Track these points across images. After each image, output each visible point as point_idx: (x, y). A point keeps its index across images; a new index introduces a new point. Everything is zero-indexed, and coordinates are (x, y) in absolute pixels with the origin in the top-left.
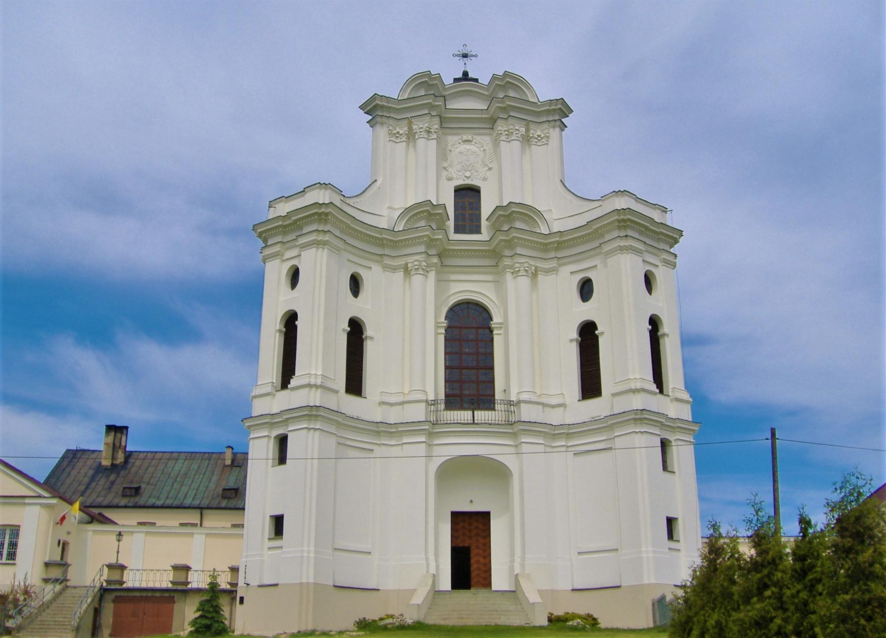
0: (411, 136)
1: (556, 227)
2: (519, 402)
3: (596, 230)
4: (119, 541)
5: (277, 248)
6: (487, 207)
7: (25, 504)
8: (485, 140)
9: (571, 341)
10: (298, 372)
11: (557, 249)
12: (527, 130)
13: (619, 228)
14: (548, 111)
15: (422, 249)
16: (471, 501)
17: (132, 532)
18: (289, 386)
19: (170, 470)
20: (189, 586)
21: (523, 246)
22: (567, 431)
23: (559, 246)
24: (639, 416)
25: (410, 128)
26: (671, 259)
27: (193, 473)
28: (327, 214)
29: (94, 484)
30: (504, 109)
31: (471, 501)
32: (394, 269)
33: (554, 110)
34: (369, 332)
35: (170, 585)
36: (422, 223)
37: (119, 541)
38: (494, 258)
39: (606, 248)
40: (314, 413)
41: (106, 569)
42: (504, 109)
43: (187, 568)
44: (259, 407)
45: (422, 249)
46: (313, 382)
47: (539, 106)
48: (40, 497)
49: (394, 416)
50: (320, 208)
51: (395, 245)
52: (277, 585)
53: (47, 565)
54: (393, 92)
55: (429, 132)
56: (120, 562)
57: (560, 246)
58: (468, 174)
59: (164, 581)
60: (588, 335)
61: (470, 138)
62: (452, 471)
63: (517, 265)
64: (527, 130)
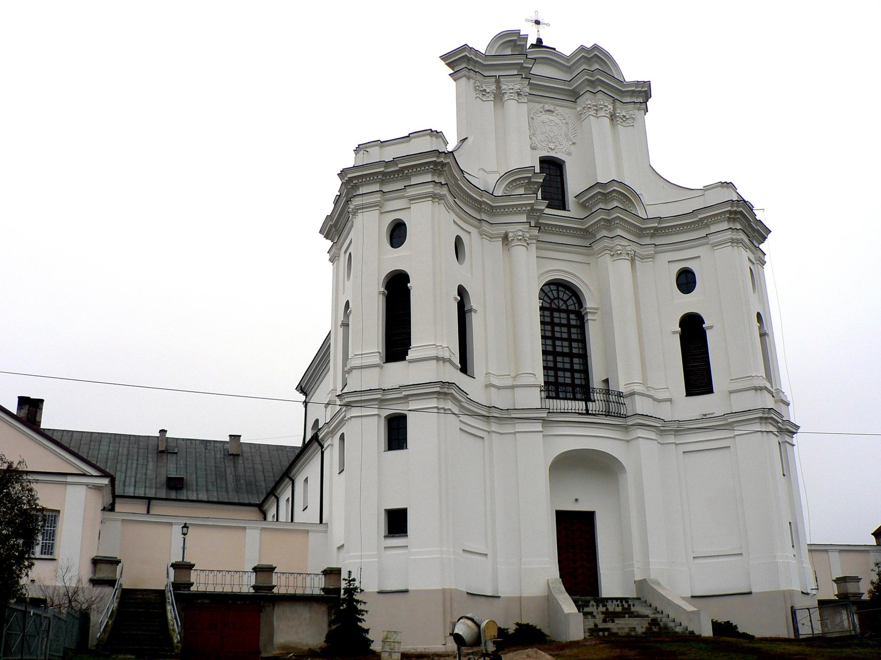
0: (499, 96)
1: (652, 213)
2: (632, 394)
3: (701, 220)
4: (185, 534)
5: (377, 198)
6: (575, 183)
7: (66, 483)
8: (564, 112)
9: (674, 333)
10: (414, 343)
11: (653, 236)
12: (615, 109)
13: (729, 220)
14: (633, 91)
15: (524, 218)
16: (576, 500)
17: (171, 524)
18: (411, 354)
19: (96, 453)
20: (193, 588)
21: (623, 229)
22: (678, 428)
23: (655, 231)
24: (766, 415)
25: (499, 87)
26: (762, 256)
27: (124, 458)
28: (443, 165)
29: (130, 461)
30: (592, 83)
31: (576, 500)
32: (491, 237)
33: (640, 92)
34: (474, 302)
35: (252, 590)
36: (521, 191)
37: (185, 534)
38: (586, 237)
40: (446, 390)
41: (172, 571)
42: (592, 83)
43: (270, 569)
44: (369, 380)
45: (524, 218)
46: (441, 354)
47: (624, 86)
48: (84, 475)
49: (500, 400)
50: (438, 157)
51: (493, 211)
52: (406, 591)
53: (96, 562)
54: (481, 46)
55: (519, 94)
56: (187, 560)
57: (657, 232)
58: (552, 146)
59: (246, 584)
61: (551, 108)
62: (567, 465)
63: (620, 248)
64: (615, 109)
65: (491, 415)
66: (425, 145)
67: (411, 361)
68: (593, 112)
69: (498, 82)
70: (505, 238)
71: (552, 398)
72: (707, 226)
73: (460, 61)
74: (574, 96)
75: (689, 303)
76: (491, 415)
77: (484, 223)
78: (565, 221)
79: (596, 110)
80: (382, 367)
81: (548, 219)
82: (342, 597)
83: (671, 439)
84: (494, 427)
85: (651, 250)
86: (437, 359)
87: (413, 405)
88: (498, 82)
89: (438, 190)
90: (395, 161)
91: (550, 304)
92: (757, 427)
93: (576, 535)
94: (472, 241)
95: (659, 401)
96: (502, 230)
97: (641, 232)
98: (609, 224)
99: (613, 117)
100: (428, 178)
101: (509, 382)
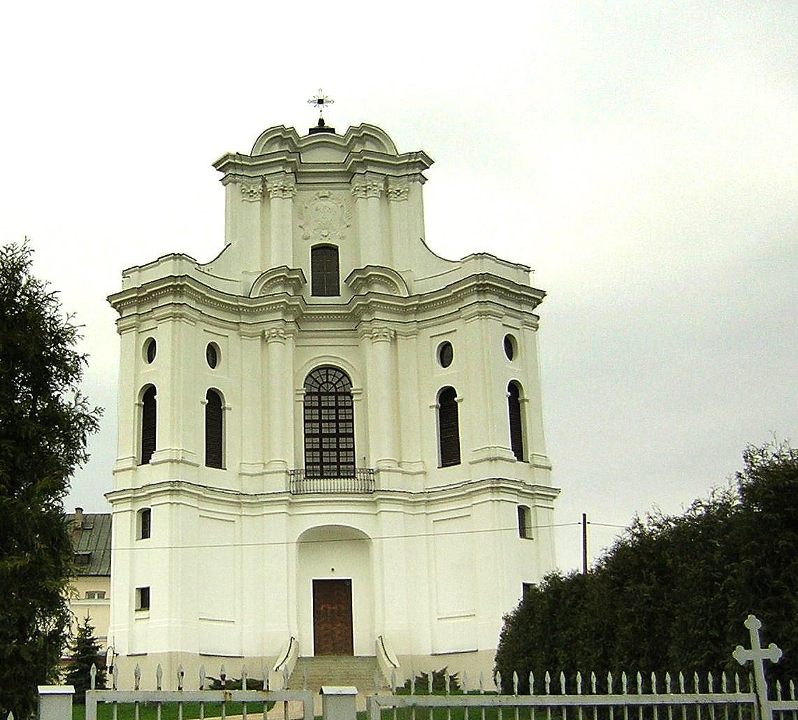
8: (341, 194)
11: (417, 312)
16: (333, 570)
21: (379, 310)
22: (427, 499)
23: (418, 308)
31: (333, 570)
39: (465, 313)
45: (279, 316)
47: (398, 160)
49: (250, 487)
54: (246, 151)
55: (283, 190)
57: (420, 309)
60: (447, 400)
61: (326, 193)
62: (315, 539)
65: (239, 499)
66: (167, 269)
67: (153, 464)
68: (361, 194)
69: (264, 181)
70: (263, 336)
71: (317, 478)
72: (462, 299)
73: (229, 166)
74: (351, 174)
75: (446, 377)
76: (239, 499)
77: (241, 325)
78: (333, 309)
79: (365, 191)
80: (136, 470)
81: (313, 309)
82: (716, 583)
83: (422, 509)
84: (245, 511)
85: (413, 327)
86: (172, 461)
87: (154, 501)
88: (264, 181)
89: (177, 311)
90: (143, 288)
91: (319, 389)
92: (489, 496)
93: (332, 601)
94: (229, 345)
95: (413, 474)
96: (259, 329)
97: (405, 311)
98: (368, 308)
99: (386, 194)
100: (170, 300)
101: (260, 469)
